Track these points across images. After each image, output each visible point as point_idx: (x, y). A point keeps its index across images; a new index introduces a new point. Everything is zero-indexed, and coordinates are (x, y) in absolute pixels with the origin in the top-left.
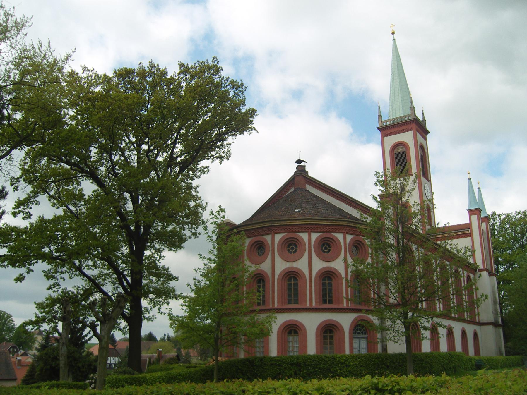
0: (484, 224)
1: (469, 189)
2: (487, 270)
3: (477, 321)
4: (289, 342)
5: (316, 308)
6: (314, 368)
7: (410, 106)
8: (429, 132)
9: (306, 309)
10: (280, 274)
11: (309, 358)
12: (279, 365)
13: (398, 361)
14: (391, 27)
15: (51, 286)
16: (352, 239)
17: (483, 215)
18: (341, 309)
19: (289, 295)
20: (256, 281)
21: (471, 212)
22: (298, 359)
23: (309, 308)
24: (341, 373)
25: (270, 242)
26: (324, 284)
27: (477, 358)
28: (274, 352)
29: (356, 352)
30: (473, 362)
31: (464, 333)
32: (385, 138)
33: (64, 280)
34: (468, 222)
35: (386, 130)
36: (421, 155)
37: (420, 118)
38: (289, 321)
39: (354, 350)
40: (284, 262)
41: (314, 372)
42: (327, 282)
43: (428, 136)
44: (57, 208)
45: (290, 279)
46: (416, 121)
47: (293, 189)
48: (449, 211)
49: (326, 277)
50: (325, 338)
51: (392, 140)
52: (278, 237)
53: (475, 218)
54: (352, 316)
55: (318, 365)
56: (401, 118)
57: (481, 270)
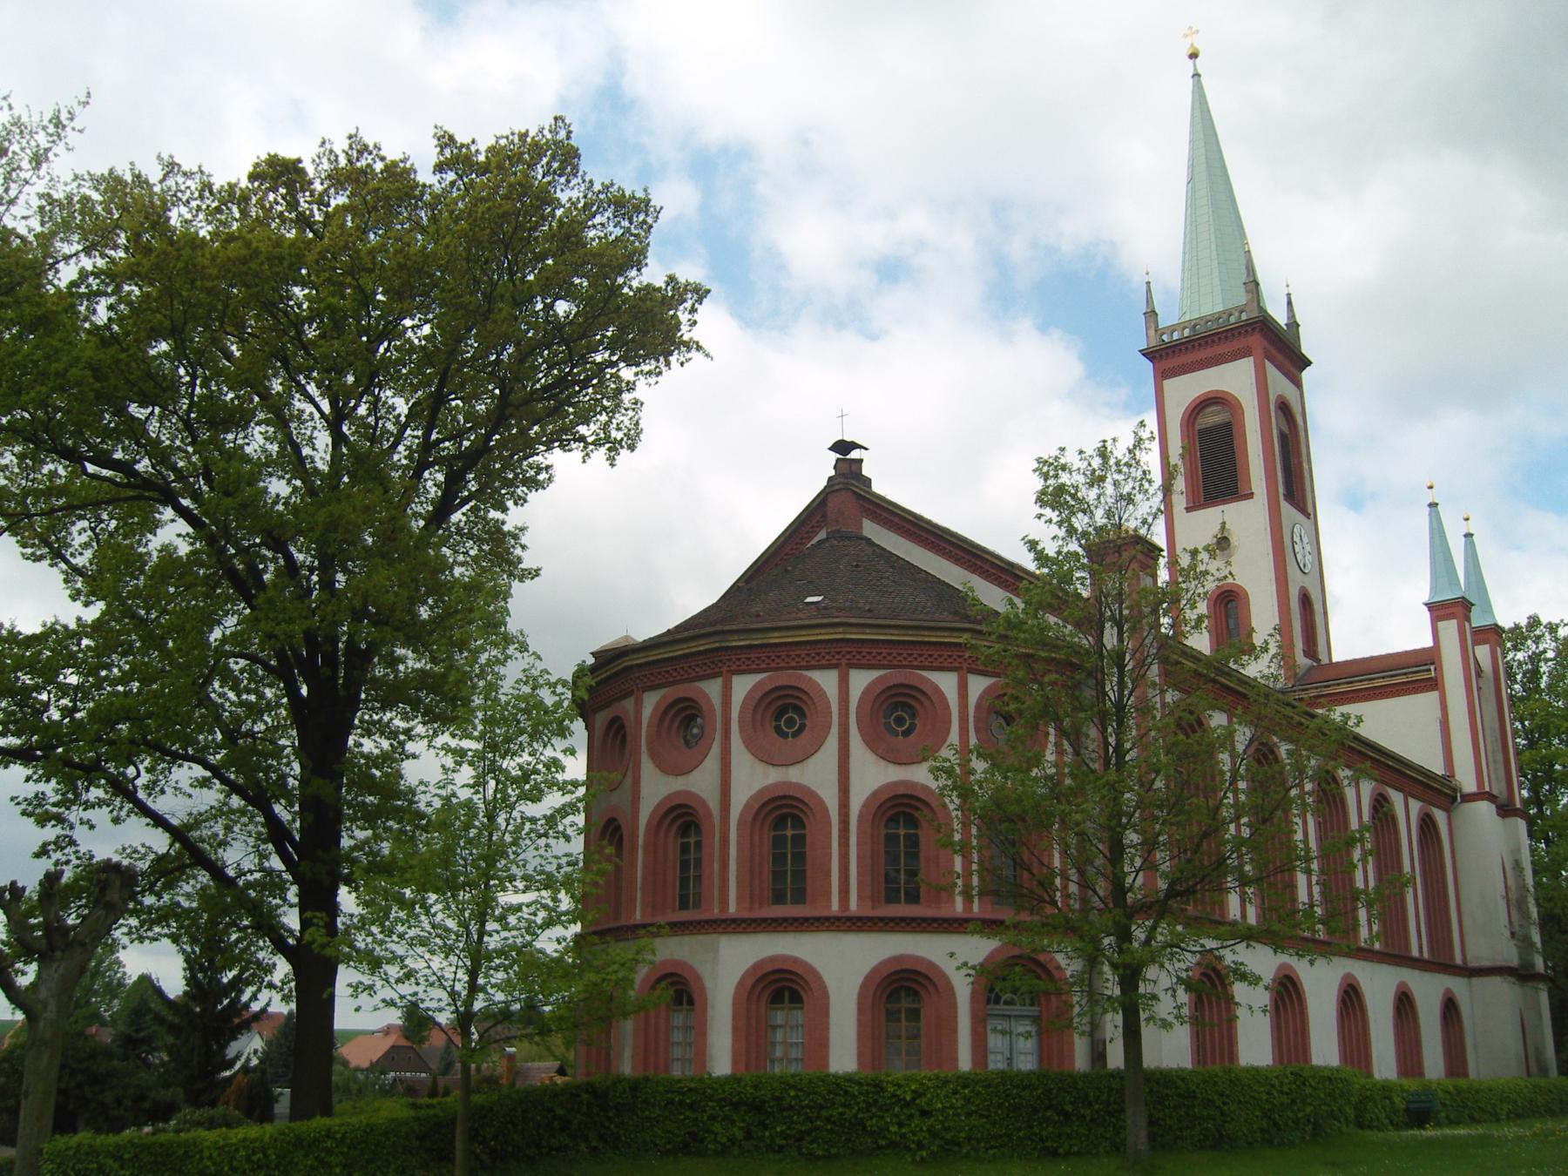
0: (1483, 652)
1: (1432, 538)
2: (1490, 797)
3: (1458, 960)
4: (774, 1028)
5: (860, 919)
6: (809, 1119)
7: (1244, 278)
8: (1307, 363)
9: (827, 919)
10: (748, 806)
11: (840, 1085)
12: (691, 1107)
13: (1104, 1097)
14: (1186, 36)
15: (45, 845)
16: (987, 691)
17: (1478, 620)
18: (945, 920)
19: (778, 876)
20: (675, 828)
21: (1439, 610)
22: (756, 1087)
23: (838, 919)
24: (903, 1136)
25: (717, 701)
26: (891, 839)
27: (1410, 1084)
28: (721, 1062)
29: (996, 1063)
30: (1397, 1100)
31: (1404, 1004)
32: (1168, 384)
33: (92, 827)
34: (1429, 643)
35: (1171, 355)
36: (1282, 436)
37: (1281, 318)
38: (772, 959)
39: (991, 1057)
40: (760, 767)
41: (809, 1132)
42: (902, 832)
43: (1306, 375)
44: (87, 604)
45: (780, 822)
46: (1264, 324)
47: (822, 535)
48: (1374, 608)
49: (898, 814)
50: (892, 1016)
51: (1187, 388)
52: (743, 686)
53: (1449, 628)
54: (977, 948)
55: (821, 1107)
56: (1217, 317)
57: (1469, 798)
